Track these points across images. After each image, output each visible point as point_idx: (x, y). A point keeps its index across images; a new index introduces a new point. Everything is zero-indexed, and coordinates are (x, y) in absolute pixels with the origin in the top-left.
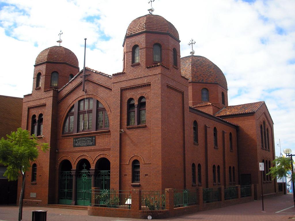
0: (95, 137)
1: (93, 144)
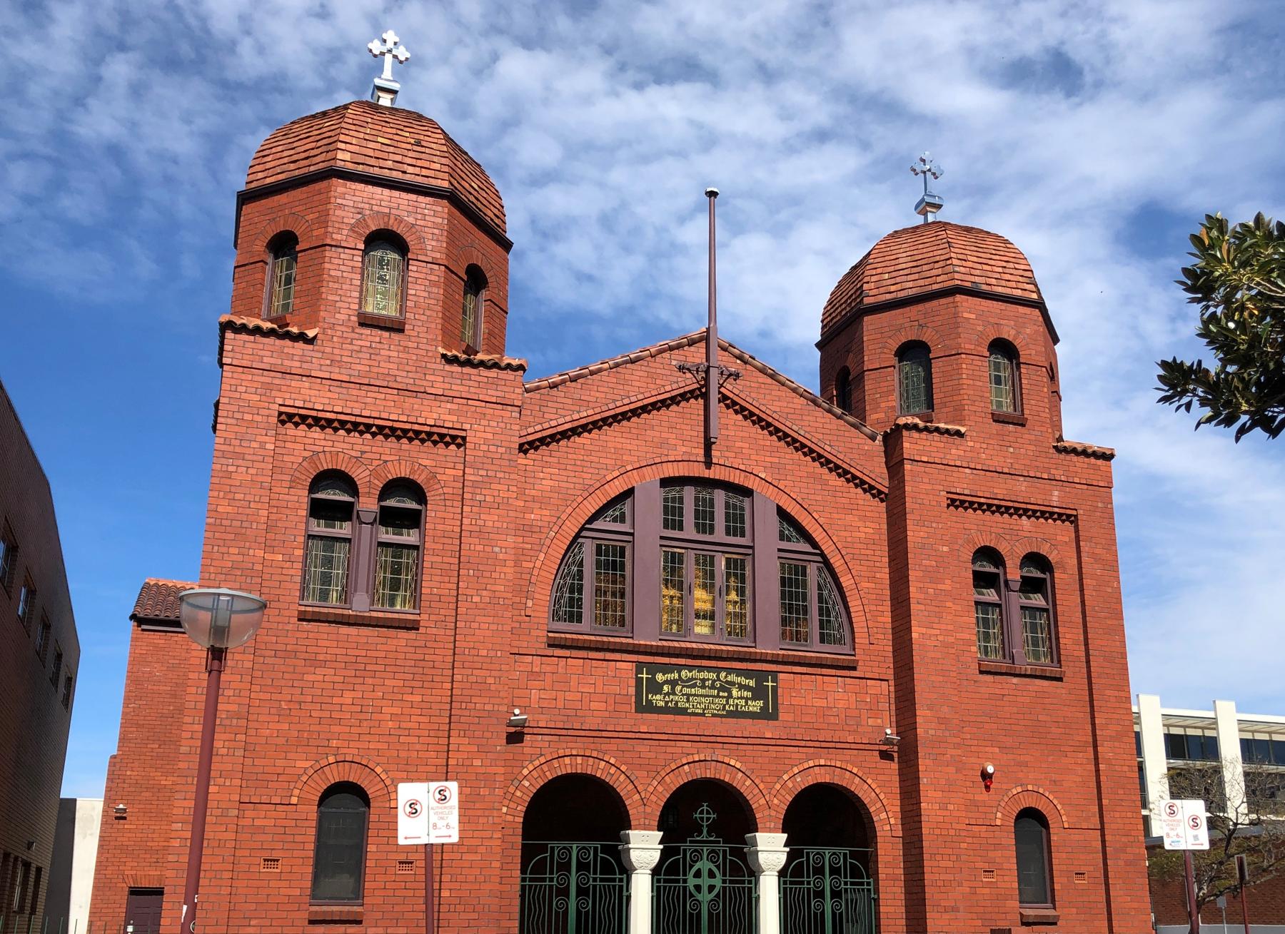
0: (774, 674)
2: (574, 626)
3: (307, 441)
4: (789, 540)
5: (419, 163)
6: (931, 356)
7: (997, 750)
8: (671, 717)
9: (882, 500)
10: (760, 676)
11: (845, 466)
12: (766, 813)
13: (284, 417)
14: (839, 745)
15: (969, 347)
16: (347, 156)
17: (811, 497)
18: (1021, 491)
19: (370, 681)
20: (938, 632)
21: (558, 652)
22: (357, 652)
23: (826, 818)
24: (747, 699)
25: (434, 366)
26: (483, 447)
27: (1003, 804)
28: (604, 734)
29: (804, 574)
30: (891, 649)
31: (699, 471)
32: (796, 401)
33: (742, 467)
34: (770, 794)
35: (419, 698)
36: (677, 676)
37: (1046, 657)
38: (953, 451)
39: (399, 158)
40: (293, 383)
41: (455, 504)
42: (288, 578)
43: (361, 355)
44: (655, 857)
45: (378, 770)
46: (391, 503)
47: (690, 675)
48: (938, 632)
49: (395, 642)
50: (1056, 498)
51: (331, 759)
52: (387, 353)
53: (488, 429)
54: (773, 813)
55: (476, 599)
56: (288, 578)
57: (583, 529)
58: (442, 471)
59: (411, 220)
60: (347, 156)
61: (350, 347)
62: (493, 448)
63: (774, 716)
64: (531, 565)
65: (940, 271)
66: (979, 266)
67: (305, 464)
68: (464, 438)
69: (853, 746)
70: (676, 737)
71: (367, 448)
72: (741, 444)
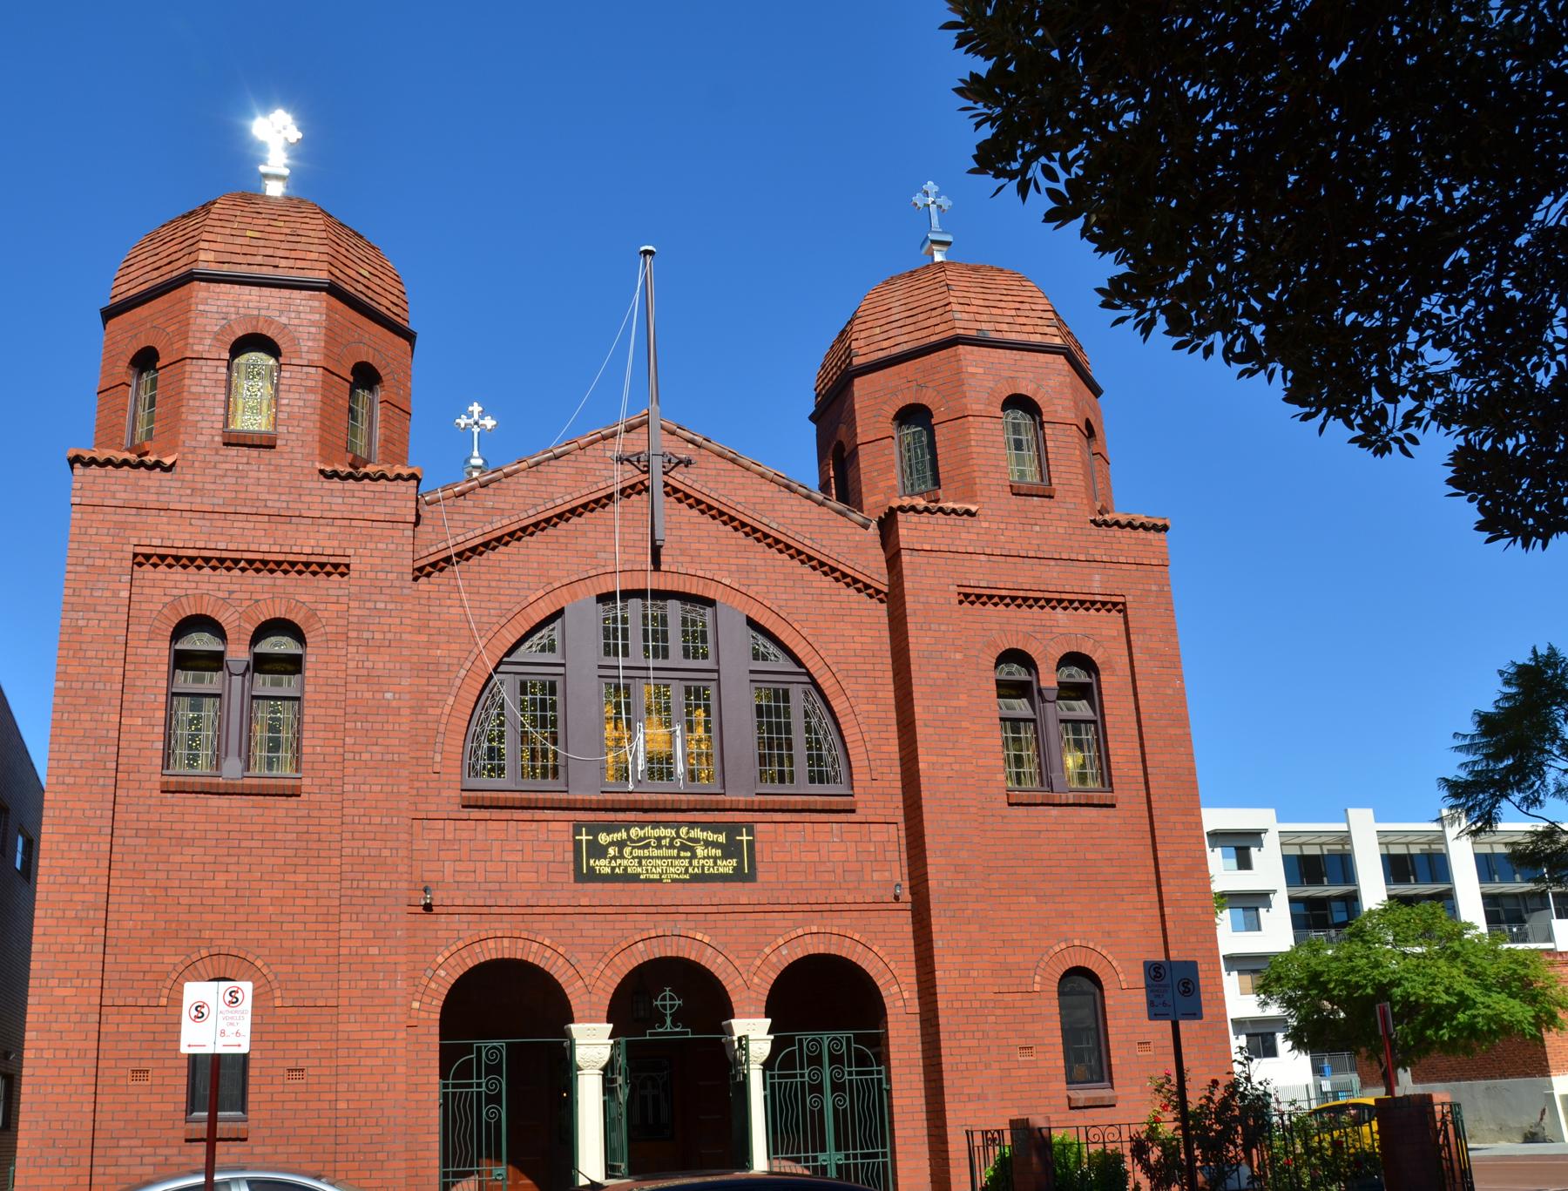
1: (738, 869)
2: (496, 782)
3: (167, 584)
4: (765, 658)
5: (293, 254)
6: (933, 421)
7: (1033, 899)
8: (619, 886)
9: (881, 601)
10: (732, 829)
11: (831, 562)
12: (745, 994)
13: (140, 559)
14: (834, 907)
15: (976, 407)
16: (211, 256)
17: (790, 603)
18: (1054, 579)
19: (246, 860)
20: (952, 760)
21: (476, 814)
22: (230, 827)
23: (823, 996)
24: (715, 858)
25: (311, 485)
26: (369, 575)
27: (1042, 965)
28: (536, 910)
29: (786, 699)
30: (899, 784)
31: (652, 582)
32: (764, 488)
33: (700, 573)
34: (748, 975)
35: (303, 878)
36: (624, 836)
37: (1095, 779)
38: (964, 535)
39: (269, 252)
40: (149, 520)
41: (340, 644)
42: (148, 744)
43: (226, 480)
44: (604, 1054)
45: (259, 963)
46: (184, 645)
47: (641, 833)
48: (952, 760)
49: (273, 813)
50: (1097, 584)
51: (204, 953)
52: (256, 474)
53: (376, 553)
54: (754, 995)
55: (366, 756)
56: (148, 744)
57: (500, 663)
58: (322, 606)
59: (284, 320)
60: (211, 256)
61: (214, 472)
62: (381, 575)
63: (751, 877)
64: (438, 711)
65: (938, 320)
66: (986, 310)
67: (165, 611)
68: (347, 566)
69: (853, 907)
70: (625, 910)
71: (236, 587)
72: (698, 546)
